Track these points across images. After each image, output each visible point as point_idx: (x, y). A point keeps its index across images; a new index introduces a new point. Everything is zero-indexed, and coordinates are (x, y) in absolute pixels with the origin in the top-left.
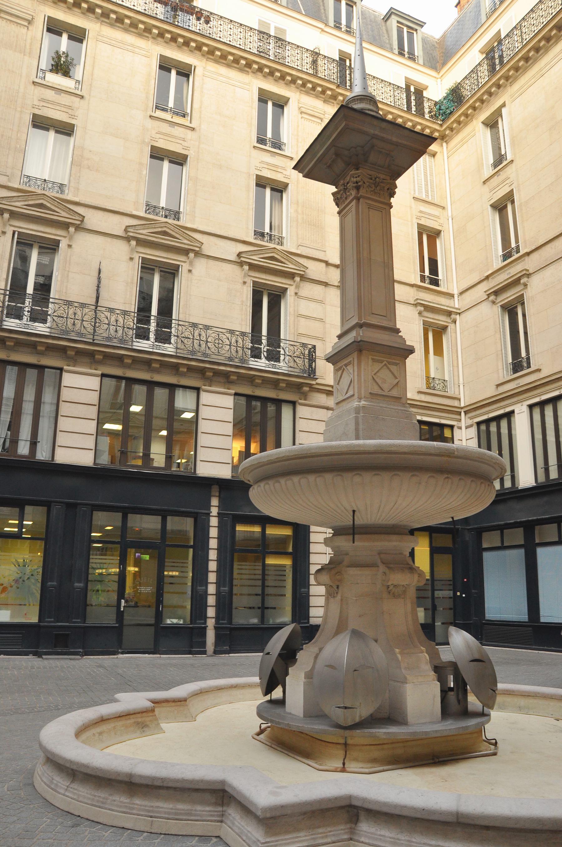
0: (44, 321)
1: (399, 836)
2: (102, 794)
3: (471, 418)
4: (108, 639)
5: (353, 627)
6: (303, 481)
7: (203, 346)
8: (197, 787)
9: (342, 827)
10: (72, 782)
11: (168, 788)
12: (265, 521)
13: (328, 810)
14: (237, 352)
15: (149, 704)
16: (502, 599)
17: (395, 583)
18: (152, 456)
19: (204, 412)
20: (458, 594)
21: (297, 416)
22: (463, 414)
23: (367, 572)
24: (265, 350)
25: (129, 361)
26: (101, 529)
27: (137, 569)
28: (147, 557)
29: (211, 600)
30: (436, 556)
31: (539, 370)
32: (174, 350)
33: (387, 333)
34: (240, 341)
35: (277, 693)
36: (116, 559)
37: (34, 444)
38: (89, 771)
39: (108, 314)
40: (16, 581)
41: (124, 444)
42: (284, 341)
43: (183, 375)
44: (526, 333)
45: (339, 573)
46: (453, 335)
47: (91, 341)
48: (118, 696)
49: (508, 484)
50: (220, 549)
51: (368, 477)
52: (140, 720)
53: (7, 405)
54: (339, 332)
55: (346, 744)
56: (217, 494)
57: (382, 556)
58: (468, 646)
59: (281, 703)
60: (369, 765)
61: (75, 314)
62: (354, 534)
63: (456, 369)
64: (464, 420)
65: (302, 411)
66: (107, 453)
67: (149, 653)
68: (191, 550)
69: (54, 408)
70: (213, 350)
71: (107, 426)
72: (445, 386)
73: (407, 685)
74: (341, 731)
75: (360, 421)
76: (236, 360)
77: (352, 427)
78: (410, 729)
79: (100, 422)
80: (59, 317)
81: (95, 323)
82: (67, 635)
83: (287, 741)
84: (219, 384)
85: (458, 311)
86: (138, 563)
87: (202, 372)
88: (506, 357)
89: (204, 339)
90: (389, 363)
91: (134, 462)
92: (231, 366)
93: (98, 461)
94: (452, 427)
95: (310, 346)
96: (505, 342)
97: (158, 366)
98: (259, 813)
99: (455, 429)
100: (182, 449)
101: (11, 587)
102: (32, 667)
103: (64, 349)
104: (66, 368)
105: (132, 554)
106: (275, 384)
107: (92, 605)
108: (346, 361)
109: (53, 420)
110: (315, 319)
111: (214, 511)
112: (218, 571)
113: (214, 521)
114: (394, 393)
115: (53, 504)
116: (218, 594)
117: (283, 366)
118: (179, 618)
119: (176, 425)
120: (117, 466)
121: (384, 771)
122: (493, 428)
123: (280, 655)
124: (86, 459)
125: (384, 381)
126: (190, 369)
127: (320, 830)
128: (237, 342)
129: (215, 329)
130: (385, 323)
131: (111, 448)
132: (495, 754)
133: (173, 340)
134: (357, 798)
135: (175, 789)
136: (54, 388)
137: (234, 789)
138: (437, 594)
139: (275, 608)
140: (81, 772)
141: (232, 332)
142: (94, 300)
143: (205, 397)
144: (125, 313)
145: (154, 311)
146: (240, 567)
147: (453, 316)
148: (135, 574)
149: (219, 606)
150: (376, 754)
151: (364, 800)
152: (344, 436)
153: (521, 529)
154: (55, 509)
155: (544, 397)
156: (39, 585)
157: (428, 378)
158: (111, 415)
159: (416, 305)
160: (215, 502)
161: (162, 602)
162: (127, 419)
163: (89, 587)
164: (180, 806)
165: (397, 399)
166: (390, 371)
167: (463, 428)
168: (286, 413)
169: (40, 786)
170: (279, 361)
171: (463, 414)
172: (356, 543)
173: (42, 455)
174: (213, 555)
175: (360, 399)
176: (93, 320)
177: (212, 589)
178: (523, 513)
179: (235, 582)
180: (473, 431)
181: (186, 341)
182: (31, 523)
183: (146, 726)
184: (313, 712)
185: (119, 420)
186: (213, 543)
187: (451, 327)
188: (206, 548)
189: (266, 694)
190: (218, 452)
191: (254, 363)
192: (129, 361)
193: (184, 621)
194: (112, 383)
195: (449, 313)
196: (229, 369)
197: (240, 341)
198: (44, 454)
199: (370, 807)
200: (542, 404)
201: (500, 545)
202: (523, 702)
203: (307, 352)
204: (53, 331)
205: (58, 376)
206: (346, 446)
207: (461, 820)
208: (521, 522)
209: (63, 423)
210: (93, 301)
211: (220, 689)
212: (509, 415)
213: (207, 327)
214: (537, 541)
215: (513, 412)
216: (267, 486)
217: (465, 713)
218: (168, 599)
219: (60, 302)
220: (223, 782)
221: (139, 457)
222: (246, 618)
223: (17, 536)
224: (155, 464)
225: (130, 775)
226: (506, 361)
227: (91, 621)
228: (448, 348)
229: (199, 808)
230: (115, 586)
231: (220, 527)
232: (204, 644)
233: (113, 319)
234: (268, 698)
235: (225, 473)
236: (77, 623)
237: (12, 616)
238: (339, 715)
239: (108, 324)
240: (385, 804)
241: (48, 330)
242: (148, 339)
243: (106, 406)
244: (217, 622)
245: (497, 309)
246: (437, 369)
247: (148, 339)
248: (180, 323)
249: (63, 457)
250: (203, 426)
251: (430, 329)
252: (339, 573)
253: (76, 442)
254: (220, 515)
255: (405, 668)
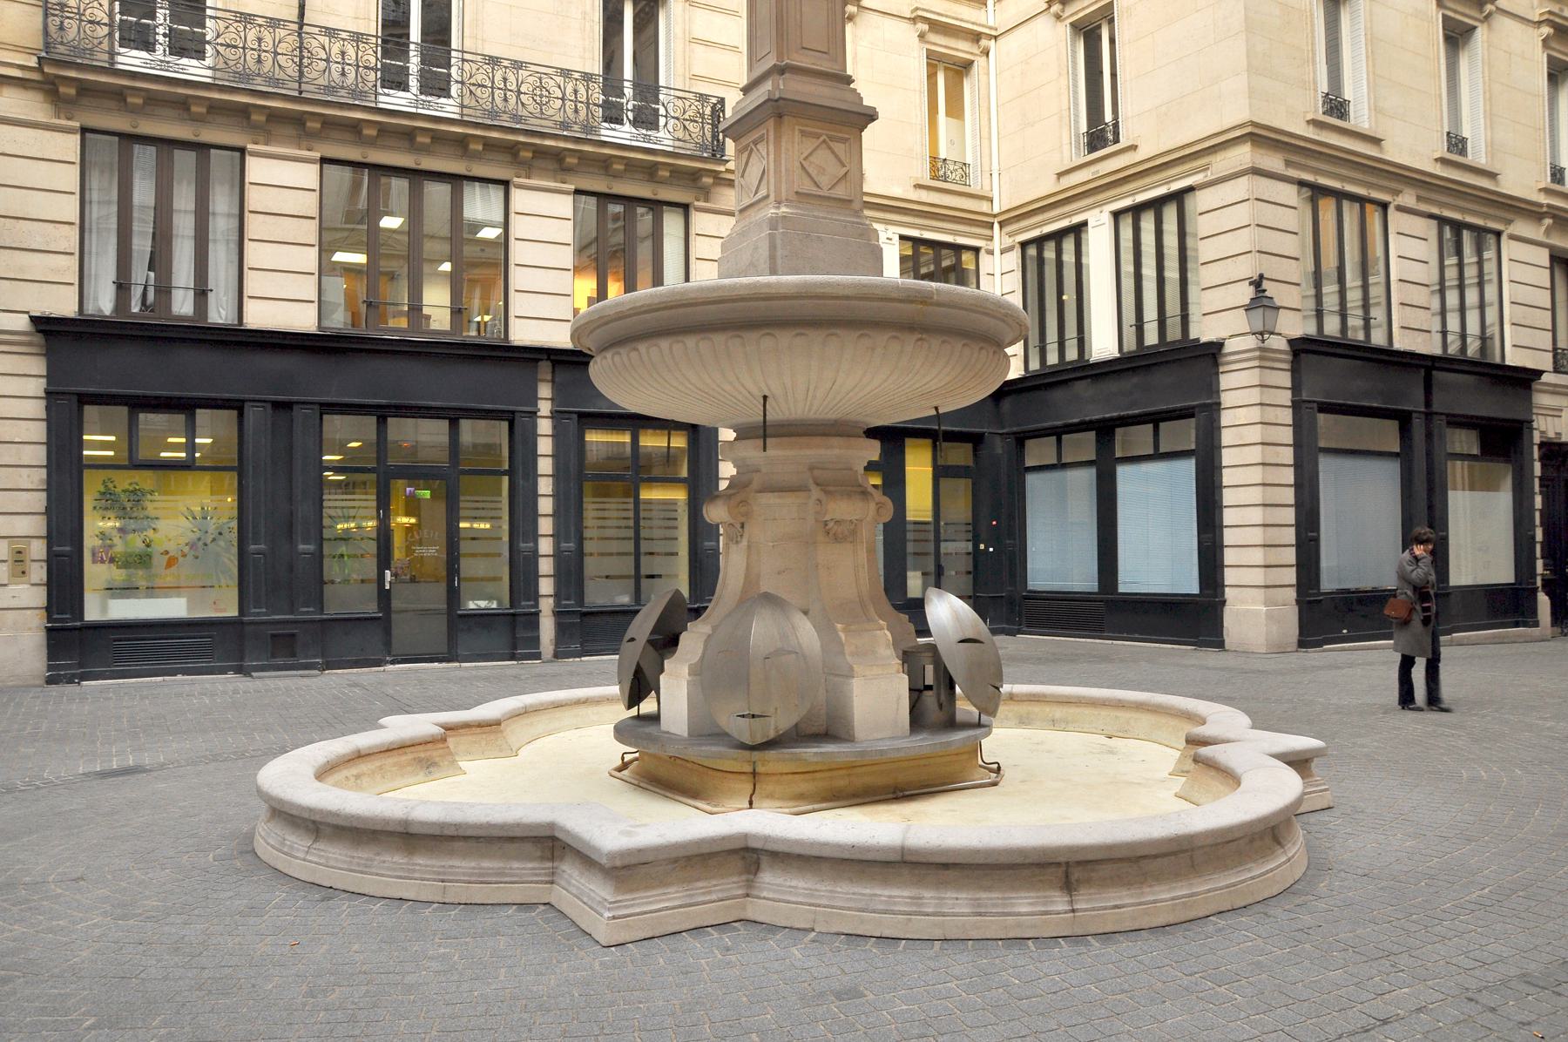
0: (200, 54)
1: (818, 886)
2: (363, 854)
3: (1010, 235)
4: (367, 638)
5: (803, 606)
6: (677, 347)
7: (512, 100)
8: (511, 834)
9: (735, 879)
10: (315, 841)
11: (466, 838)
12: (637, 422)
13: (712, 855)
14: (576, 111)
15: (438, 730)
16: (1057, 556)
17: (838, 517)
18: (426, 311)
19: (519, 227)
20: (982, 547)
21: (692, 232)
22: (996, 226)
23: (790, 500)
24: (630, 106)
25: (372, 132)
26: (341, 448)
27: (413, 520)
28: (427, 494)
29: (546, 566)
30: (943, 482)
31: (1133, 148)
32: (457, 110)
33: (829, 83)
34: (582, 90)
35: (648, 706)
36: (371, 500)
37: (201, 293)
38: (341, 823)
39: (325, 40)
40: (192, 545)
41: (372, 289)
42: (664, 91)
43: (475, 156)
44: (1114, 75)
45: (744, 502)
46: (983, 78)
47: (296, 94)
48: (382, 721)
49: (1072, 354)
50: (558, 476)
51: (785, 338)
52: (424, 755)
53: (144, 221)
54: (744, 82)
55: (754, 774)
56: (549, 377)
57: (816, 472)
58: (957, 617)
59: (655, 718)
60: (791, 804)
61: (260, 40)
62: (765, 437)
63: (986, 142)
64: (999, 238)
65: (700, 221)
66: (342, 308)
67: (440, 661)
68: (506, 479)
69: (235, 223)
70: (531, 108)
71: (339, 257)
72: (966, 175)
73: (854, 681)
74: (746, 753)
75: (779, 242)
76: (576, 128)
77: (764, 252)
78: (857, 748)
79: (325, 250)
80: (228, 46)
81: (302, 58)
82: (293, 635)
83: (661, 773)
84: (544, 173)
85: (994, 33)
86: (413, 507)
87: (512, 150)
88: (1077, 122)
89: (514, 87)
90: (832, 138)
91: (392, 323)
92: (566, 138)
93: (326, 323)
94: (976, 250)
95: (714, 100)
96: (1076, 92)
97: (428, 140)
98: (604, 861)
99: (982, 254)
100: (486, 297)
101: (184, 555)
102: (235, 692)
103: (243, 112)
104: (250, 147)
105: (402, 489)
106: (649, 171)
107: (333, 582)
108: (755, 135)
109: (234, 247)
110: (723, 47)
111: (545, 408)
112: (556, 515)
113: (545, 426)
114: (840, 192)
115: (247, 405)
116: (558, 555)
117: (664, 139)
118: (490, 599)
119: (469, 251)
120: (362, 331)
121: (814, 811)
122: (1050, 253)
123: (650, 642)
124: (303, 320)
125: (822, 171)
126: (489, 145)
127: (700, 884)
128: (576, 92)
129: (533, 68)
130: (825, 66)
131: (350, 297)
132: (995, 784)
133: (455, 89)
134: (755, 837)
135: (477, 838)
136: (232, 186)
137: (568, 832)
138: (945, 547)
139: (660, 576)
140: (329, 825)
141: (566, 73)
142: (296, 11)
143: (520, 199)
144: (358, 38)
145: (415, 33)
146: (601, 514)
147: (984, 42)
148: (409, 529)
149: (560, 576)
150: (804, 786)
151: (767, 838)
152: (752, 268)
153: (1092, 435)
154: (251, 413)
155: (1141, 198)
156: (235, 550)
157: (934, 159)
158: (346, 234)
159: (914, 20)
160: (545, 391)
161: (458, 572)
162: (373, 241)
163: (326, 551)
164: (486, 864)
165: (846, 202)
166: (833, 152)
167: (997, 252)
168: (672, 224)
169: (261, 847)
170: (657, 129)
171: (996, 226)
172: (770, 452)
173: (220, 313)
174: (545, 486)
175: (779, 203)
176: (297, 53)
177: (545, 546)
178: (1092, 403)
179: (587, 534)
180: (1014, 259)
181: (478, 92)
182: (209, 441)
183: (434, 764)
184: (706, 731)
185: (360, 243)
186: (545, 466)
187: (980, 62)
188: (532, 475)
189: (630, 707)
190: (547, 300)
191: (609, 133)
192: (372, 132)
193: (500, 603)
194: (346, 173)
195: (976, 37)
196: (562, 144)
197: (582, 90)
198: (223, 313)
199: (775, 847)
200: (1137, 210)
201: (1054, 461)
202: (1059, 712)
203: (708, 111)
204: (219, 74)
205: (237, 161)
206: (748, 286)
207: (908, 858)
208: (1091, 422)
209: (255, 254)
210: (293, 14)
211: (558, 705)
212: (1078, 230)
213: (518, 65)
214: (1118, 454)
215: (1085, 224)
216: (617, 358)
217: (951, 724)
218: (468, 567)
219: (227, 15)
220: (552, 826)
221: (401, 314)
222: (604, 594)
223: (185, 466)
224: (434, 326)
225: (406, 823)
226: (1077, 128)
227: (332, 610)
228: (973, 103)
229: (516, 865)
230: (372, 547)
231: (556, 436)
232: (535, 641)
233: (336, 49)
234: (634, 712)
235: (560, 338)
236: (307, 612)
237: (189, 609)
238: (743, 730)
239: (327, 60)
240: (798, 842)
241: (209, 73)
242: (406, 88)
243: (337, 219)
244: (557, 604)
245: (1064, 30)
246: (952, 142)
247: (406, 88)
248: (467, 56)
249: (259, 317)
250: (518, 252)
251: (941, 66)
252: (744, 502)
253: (282, 288)
254: (555, 415)
255: (852, 654)
